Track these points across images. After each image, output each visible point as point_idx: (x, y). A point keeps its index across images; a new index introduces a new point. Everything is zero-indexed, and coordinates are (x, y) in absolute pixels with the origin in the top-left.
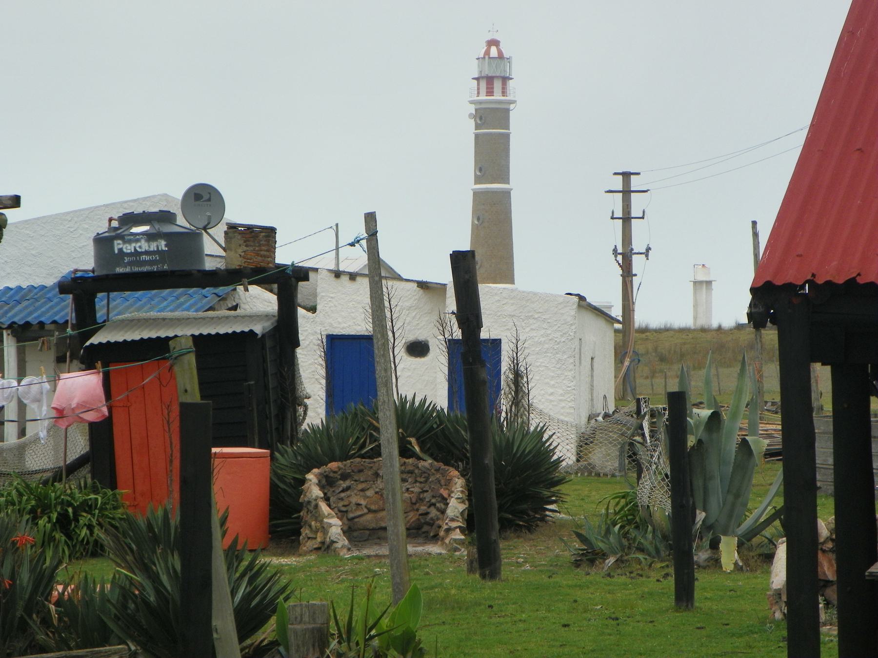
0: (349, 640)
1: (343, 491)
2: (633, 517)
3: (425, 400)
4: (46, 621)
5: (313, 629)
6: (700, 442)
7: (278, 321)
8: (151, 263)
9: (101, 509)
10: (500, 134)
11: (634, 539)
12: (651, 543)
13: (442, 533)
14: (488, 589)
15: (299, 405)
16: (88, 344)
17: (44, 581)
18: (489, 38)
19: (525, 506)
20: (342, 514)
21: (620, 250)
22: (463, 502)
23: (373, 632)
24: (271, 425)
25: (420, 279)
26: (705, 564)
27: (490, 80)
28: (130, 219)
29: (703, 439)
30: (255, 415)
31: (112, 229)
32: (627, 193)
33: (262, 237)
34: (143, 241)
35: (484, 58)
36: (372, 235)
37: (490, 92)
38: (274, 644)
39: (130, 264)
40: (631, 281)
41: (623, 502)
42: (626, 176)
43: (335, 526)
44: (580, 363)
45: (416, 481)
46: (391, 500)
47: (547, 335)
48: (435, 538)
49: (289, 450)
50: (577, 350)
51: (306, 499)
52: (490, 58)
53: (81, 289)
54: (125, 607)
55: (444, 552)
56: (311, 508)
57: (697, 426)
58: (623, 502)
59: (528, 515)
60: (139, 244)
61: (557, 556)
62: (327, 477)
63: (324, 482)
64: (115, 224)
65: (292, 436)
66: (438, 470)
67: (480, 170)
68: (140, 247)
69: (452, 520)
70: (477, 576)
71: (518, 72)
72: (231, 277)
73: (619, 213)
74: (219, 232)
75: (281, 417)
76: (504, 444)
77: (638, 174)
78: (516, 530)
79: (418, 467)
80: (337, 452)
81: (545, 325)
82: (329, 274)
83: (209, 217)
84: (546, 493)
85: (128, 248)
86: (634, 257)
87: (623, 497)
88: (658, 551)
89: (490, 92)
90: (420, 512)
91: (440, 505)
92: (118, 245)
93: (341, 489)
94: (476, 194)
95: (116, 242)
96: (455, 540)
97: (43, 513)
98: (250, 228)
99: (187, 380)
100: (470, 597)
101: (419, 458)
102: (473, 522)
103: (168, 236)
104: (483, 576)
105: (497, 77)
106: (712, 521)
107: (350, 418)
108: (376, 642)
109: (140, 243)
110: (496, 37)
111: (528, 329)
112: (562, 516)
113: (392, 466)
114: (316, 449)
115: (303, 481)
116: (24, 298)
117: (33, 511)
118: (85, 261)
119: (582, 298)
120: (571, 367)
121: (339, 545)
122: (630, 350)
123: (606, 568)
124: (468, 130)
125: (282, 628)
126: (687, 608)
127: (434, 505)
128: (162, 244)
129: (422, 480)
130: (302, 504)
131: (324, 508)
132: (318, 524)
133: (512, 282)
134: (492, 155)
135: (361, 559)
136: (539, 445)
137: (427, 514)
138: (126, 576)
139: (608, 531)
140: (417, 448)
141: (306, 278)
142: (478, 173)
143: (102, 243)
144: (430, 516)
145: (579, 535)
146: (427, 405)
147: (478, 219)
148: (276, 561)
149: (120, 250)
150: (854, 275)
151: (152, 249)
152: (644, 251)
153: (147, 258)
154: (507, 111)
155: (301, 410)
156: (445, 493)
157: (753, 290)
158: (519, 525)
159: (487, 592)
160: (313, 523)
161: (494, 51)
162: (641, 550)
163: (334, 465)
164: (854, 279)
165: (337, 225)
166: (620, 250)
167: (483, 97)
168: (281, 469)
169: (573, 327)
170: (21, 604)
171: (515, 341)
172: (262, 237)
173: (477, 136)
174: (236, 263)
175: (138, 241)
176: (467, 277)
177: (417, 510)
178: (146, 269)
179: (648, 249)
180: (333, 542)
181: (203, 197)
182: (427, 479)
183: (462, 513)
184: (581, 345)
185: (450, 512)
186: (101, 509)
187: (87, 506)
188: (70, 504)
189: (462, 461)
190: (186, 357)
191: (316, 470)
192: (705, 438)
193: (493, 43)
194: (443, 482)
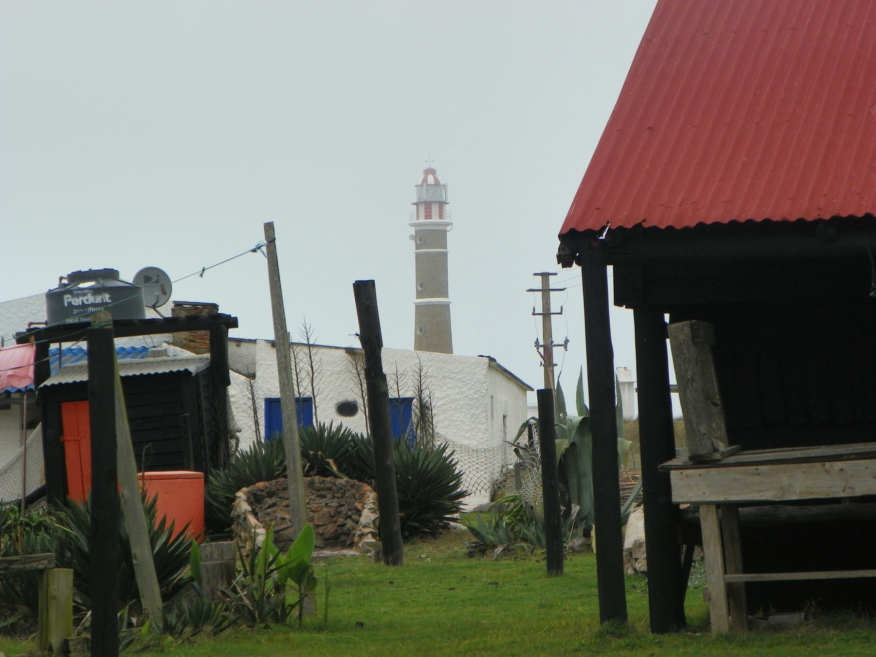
0: (253, 574)
1: (269, 507)
3: (341, 426)
5: (221, 565)
6: (573, 445)
7: (211, 363)
11: (520, 531)
12: (534, 534)
13: (356, 539)
14: (391, 572)
15: (231, 438)
16: (42, 385)
19: (429, 515)
21: (541, 343)
22: (375, 512)
23: (273, 567)
24: (205, 454)
25: (348, 346)
26: (579, 549)
27: (428, 205)
28: (78, 277)
29: (576, 442)
30: (191, 443)
31: (62, 285)
32: (546, 291)
34: (89, 295)
35: (422, 185)
36: (271, 242)
37: (428, 215)
38: (191, 579)
40: (553, 370)
44: (492, 418)
45: (334, 497)
46: (292, 467)
47: (463, 393)
48: (351, 545)
49: (222, 474)
50: (489, 406)
51: (236, 513)
52: (427, 185)
55: (357, 554)
56: (241, 521)
57: (570, 430)
58: (513, 504)
59: (433, 523)
60: (86, 298)
61: (456, 552)
63: (252, 499)
65: (225, 464)
66: (352, 486)
67: (421, 286)
68: (87, 300)
69: (365, 526)
70: (382, 563)
71: (452, 196)
73: (539, 310)
75: (215, 448)
76: (410, 460)
77: (556, 274)
78: (422, 537)
79: (335, 485)
80: (264, 473)
81: (460, 384)
82: (266, 344)
85: (77, 302)
86: (555, 349)
87: (513, 501)
88: (539, 540)
89: (428, 215)
90: (338, 524)
92: (67, 299)
93: (267, 505)
94: (418, 307)
95: (65, 296)
96: (367, 543)
100: (375, 578)
101: (336, 477)
102: (383, 530)
103: (111, 290)
104: (387, 563)
107: (275, 444)
108: (275, 575)
109: (86, 297)
111: (445, 388)
113: (292, 439)
114: (245, 471)
118: (41, 316)
119: (492, 360)
120: (484, 420)
123: (495, 556)
125: (196, 569)
126: (557, 575)
127: (350, 517)
128: (107, 297)
129: (339, 495)
130: (233, 518)
131: (252, 520)
132: (247, 535)
136: (441, 461)
137: (344, 525)
138: (64, 531)
140: (335, 468)
142: (420, 289)
144: (347, 527)
146: (342, 432)
147: (421, 330)
149: (70, 303)
150: (640, 221)
151: (97, 302)
152: (563, 343)
153: (94, 310)
154: (445, 232)
155: (233, 442)
156: (358, 505)
157: (561, 236)
158: (425, 533)
160: (242, 534)
161: (431, 179)
162: (525, 539)
163: (261, 485)
164: (640, 224)
166: (541, 343)
167: (422, 220)
168: (214, 490)
169: (485, 385)
171: (418, 371)
173: (418, 256)
175: (84, 295)
176: (368, 303)
177: (336, 522)
179: (567, 341)
182: (344, 494)
183: (374, 521)
184: (492, 402)
185: (363, 520)
189: (373, 478)
191: (245, 489)
192: (577, 441)
193: (430, 171)
194: (357, 496)
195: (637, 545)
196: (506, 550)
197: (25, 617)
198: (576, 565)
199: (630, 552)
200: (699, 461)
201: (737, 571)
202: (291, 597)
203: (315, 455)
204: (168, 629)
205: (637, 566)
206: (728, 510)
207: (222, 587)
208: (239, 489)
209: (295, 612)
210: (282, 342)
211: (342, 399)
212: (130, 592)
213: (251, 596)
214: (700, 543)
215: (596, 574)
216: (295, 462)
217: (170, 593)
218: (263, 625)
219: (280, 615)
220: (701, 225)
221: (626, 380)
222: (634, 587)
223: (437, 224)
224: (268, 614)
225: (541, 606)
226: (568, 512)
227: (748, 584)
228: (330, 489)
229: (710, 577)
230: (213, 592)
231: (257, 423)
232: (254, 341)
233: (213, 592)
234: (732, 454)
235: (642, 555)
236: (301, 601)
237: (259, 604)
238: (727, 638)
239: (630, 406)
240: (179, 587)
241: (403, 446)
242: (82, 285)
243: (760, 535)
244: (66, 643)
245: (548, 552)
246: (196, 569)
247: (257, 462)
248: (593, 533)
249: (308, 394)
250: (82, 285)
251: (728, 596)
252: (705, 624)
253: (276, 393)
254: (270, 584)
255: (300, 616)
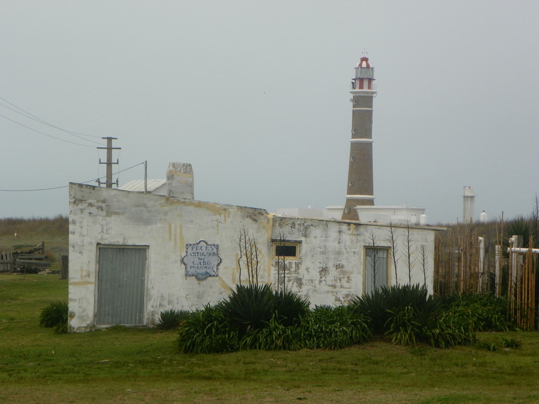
10: (366, 111)
18: (362, 57)
27: (361, 80)
32: (110, 149)
37: (361, 87)
42: (110, 139)
73: (104, 160)
77: (116, 139)
89: (361, 87)
94: (353, 144)
105: (366, 79)
110: (366, 56)
124: (349, 108)
130: (509, 253)
134: (362, 123)
142: (354, 133)
154: (371, 98)
165: (146, 162)
167: (357, 90)
173: (354, 111)
193: (365, 59)
221: (469, 195)
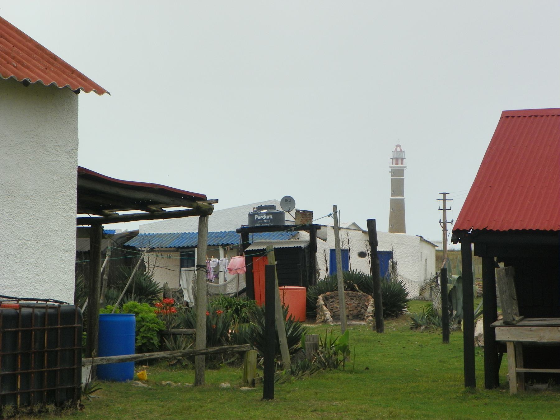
2: (432, 313)
4: (227, 340)
6: (454, 287)
8: (267, 223)
9: (249, 307)
13: (365, 318)
17: (226, 327)
20: (331, 310)
21: (442, 221)
27: (397, 159)
28: (260, 208)
32: (444, 200)
33: (308, 214)
36: (335, 212)
37: (397, 163)
38: (301, 348)
39: (260, 223)
41: (429, 308)
42: (444, 194)
43: (328, 314)
53: (244, 232)
54: (252, 335)
62: (326, 297)
64: (255, 209)
66: (364, 296)
71: (407, 156)
72: (298, 228)
74: (293, 213)
75: (311, 277)
83: (290, 208)
84: (402, 304)
85: (260, 218)
89: (397, 163)
91: (365, 308)
92: (256, 216)
94: (392, 200)
97: (230, 307)
98: (304, 211)
99: (272, 260)
100: (373, 338)
101: (358, 292)
102: (376, 314)
103: (272, 214)
104: (378, 332)
106: (458, 314)
108: (334, 348)
109: (263, 216)
112: (409, 313)
115: (317, 299)
116: (227, 235)
117: (227, 307)
118: (245, 222)
119: (422, 237)
121: (329, 321)
122: (446, 257)
124: (389, 177)
125: (303, 343)
126: (447, 343)
131: (324, 308)
133: (404, 231)
134: (398, 187)
135: (337, 325)
139: (422, 318)
140: (357, 288)
141: (320, 228)
143: (251, 216)
145: (412, 319)
148: (307, 325)
154: (403, 170)
156: (367, 304)
159: (379, 337)
161: (398, 149)
162: (434, 324)
163: (328, 293)
166: (442, 221)
167: (394, 165)
170: (219, 334)
172: (308, 214)
173: (392, 179)
174: (299, 223)
178: (265, 225)
180: (327, 320)
181: (288, 201)
183: (373, 311)
185: (368, 310)
186: (249, 307)
187: (245, 306)
188: (239, 305)
190: (271, 252)
192: (456, 285)
193: (398, 146)
195: (480, 335)
196: (426, 328)
197: (238, 359)
198: (454, 337)
199: (477, 338)
200: (507, 324)
201: (521, 367)
202: (340, 357)
203: (350, 283)
204: (293, 373)
205: (480, 344)
206: (518, 345)
207: (313, 353)
208: (319, 295)
209: (342, 364)
210: (337, 228)
211: (360, 251)
212: (278, 351)
213: (324, 357)
214: (506, 352)
215: (463, 342)
216: (341, 285)
217: (293, 352)
218: (329, 369)
219: (336, 366)
220: (510, 230)
222: (478, 353)
223: (400, 167)
224: (331, 364)
225: (441, 361)
226: (452, 314)
227: (525, 373)
228: (355, 296)
229: (509, 366)
230: (310, 354)
231: (327, 268)
232: (326, 226)
233: (310, 354)
234: (521, 320)
235: (482, 339)
236: (344, 360)
237: (328, 360)
238: (516, 396)
239: (478, 286)
240: (296, 351)
241: (385, 281)
242: (262, 212)
243: (530, 353)
244: (254, 380)
245: (443, 330)
246: (303, 343)
247: (327, 284)
248: (462, 323)
249: (347, 248)
250: (262, 212)
251: (517, 376)
252: (506, 386)
253: (334, 248)
254: (332, 351)
255: (344, 366)
